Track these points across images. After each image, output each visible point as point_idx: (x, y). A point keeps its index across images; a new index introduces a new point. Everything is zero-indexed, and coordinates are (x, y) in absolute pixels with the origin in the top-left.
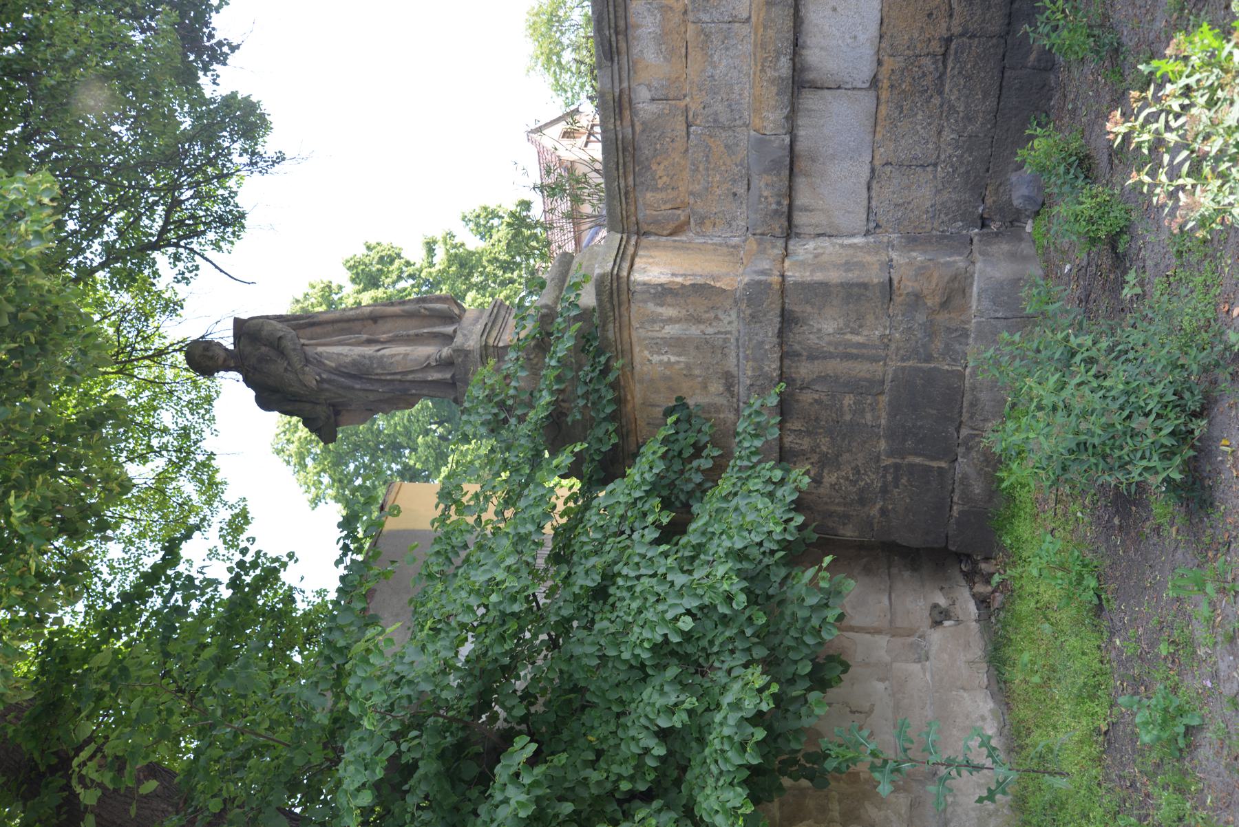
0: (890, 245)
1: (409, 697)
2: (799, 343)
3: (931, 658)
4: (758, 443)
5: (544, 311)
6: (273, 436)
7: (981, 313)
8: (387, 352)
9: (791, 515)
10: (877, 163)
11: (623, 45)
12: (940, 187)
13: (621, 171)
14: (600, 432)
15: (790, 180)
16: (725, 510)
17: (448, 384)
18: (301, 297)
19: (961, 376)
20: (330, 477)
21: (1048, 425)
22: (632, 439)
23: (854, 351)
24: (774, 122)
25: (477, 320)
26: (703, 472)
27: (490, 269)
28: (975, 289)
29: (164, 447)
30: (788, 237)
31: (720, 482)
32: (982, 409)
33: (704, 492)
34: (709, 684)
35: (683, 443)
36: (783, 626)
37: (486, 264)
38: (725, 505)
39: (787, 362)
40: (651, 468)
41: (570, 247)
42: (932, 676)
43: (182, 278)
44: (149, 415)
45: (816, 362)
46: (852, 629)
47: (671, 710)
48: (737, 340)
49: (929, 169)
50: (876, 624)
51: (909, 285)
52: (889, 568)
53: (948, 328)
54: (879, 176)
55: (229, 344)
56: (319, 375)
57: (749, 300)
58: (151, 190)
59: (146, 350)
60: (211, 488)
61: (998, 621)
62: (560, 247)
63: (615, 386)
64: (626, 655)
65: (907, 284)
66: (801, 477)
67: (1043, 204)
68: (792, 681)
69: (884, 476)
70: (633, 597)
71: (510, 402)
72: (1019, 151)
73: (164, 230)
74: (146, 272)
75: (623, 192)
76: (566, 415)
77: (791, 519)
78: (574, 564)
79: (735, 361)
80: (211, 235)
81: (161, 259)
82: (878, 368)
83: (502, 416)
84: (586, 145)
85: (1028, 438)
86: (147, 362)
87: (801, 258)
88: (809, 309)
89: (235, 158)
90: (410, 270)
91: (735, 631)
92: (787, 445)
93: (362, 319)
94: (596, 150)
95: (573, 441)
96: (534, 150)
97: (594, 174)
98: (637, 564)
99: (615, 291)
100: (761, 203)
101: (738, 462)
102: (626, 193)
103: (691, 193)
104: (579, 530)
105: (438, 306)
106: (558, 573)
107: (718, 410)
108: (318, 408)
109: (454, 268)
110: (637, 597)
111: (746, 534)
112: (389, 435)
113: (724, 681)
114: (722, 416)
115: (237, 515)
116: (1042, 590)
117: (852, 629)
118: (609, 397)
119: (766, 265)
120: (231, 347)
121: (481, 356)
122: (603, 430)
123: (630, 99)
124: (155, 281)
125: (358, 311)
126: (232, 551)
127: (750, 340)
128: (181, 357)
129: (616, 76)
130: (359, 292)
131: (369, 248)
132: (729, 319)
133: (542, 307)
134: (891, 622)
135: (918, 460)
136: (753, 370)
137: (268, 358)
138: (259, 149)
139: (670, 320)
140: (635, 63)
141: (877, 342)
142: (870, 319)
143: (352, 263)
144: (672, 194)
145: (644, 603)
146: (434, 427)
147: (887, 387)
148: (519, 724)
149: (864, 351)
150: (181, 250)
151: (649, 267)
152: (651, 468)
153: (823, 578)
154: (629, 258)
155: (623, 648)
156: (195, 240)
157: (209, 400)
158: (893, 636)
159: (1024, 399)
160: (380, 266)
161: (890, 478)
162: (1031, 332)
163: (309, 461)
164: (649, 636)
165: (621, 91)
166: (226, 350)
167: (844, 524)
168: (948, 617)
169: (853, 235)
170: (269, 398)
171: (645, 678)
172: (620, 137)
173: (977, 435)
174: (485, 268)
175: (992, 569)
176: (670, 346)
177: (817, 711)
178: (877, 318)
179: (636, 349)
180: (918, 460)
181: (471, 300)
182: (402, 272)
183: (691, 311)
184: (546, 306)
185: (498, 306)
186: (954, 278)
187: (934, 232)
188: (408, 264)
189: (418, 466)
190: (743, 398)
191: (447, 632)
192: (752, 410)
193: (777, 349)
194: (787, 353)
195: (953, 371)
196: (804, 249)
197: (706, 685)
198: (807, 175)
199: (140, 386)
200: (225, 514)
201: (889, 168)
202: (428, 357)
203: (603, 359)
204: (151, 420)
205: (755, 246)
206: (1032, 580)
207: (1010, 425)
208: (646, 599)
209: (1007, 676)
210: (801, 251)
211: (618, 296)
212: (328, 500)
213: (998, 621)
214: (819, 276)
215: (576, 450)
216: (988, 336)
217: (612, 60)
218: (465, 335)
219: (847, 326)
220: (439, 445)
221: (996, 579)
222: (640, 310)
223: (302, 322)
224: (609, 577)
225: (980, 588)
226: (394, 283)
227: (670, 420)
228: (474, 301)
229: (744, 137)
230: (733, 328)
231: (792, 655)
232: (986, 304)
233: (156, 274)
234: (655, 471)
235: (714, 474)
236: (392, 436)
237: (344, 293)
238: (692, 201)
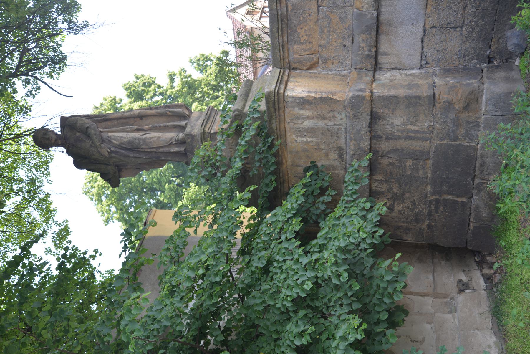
0: (434, 74)
1: (158, 329)
2: (381, 130)
3: (458, 311)
4: (356, 187)
5: (237, 113)
6: (83, 184)
7: (487, 113)
8: (148, 136)
9: (376, 229)
10: (427, 26)
12: (464, 39)
13: (280, 33)
14: (267, 181)
15: (377, 38)
16: (338, 225)
17: (181, 154)
18: (98, 105)
19: (475, 149)
20: (116, 207)
21: (527, 176)
22: (286, 185)
23: (413, 135)
24: (368, 3)
25: (199, 118)
26: (326, 203)
27: (206, 89)
28: (484, 99)
29: (20, 190)
30: (375, 70)
31: (336, 209)
32: (488, 168)
33: (326, 215)
34: (329, 324)
35: (314, 187)
36: (372, 292)
37: (203, 86)
38: (337, 222)
39: (374, 141)
40: (297, 201)
41: (251, 77)
42: (459, 321)
43: (30, 94)
44: (11, 172)
45: (390, 141)
46: (411, 293)
47: (301, 335)
48: (345, 129)
49: (458, 29)
50: (425, 291)
51: (445, 97)
52: (433, 259)
53: (468, 122)
54: (428, 34)
55: (58, 131)
56: (110, 149)
57: (352, 106)
58: (12, 42)
59: (9, 135)
60: (48, 213)
61: (498, 290)
62: (245, 77)
63: (276, 155)
64: (279, 306)
65: (444, 96)
66: (381, 207)
67: (526, 48)
68: (377, 323)
69: (430, 206)
70: (282, 273)
71: (218, 164)
72: (512, 17)
73: (19, 66)
74: (9, 90)
75: (281, 44)
76: (249, 171)
77: (376, 232)
78: (253, 255)
79: (344, 141)
80: (47, 69)
81: (18, 83)
82: (427, 144)
83: (214, 172)
84: (260, 19)
85: (515, 184)
86: (10, 142)
87: (382, 82)
88: (386, 111)
89: (60, 25)
90: (161, 90)
91: (342, 294)
92: (374, 188)
93: (134, 117)
94: (266, 22)
95: (249, 185)
96: (230, 22)
97: (265, 35)
98: (284, 253)
99: (276, 102)
100: (359, 50)
101: (346, 198)
102: (283, 46)
103: (320, 45)
104: (256, 236)
105: (177, 110)
106: (244, 260)
107: (334, 168)
108: (109, 167)
109: (185, 89)
110: (284, 272)
111: (347, 238)
112: (149, 184)
113: (336, 322)
114: (336, 172)
115: (63, 230)
116: (524, 272)
117: (411, 293)
118: (273, 161)
119: (362, 86)
120: (60, 133)
121: (201, 138)
122: (269, 180)
124: (14, 95)
125: (132, 113)
126: (59, 250)
127: (353, 129)
128: (30, 139)
130: (131, 103)
131: (137, 78)
132: (341, 117)
133: (235, 111)
134: (434, 290)
135: (449, 197)
136: (355, 145)
137: (79, 139)
138: (74, 20)
139: (308, 118)
141: (426, 130)
142: (422, 116)
143: (128, 86)
144: (309, 46)
145: (288, 275)
146: (174, 179)
147: (431, 155)
148: (222, 346)
149: (418, 135)
150: (30, 78)
151: (296, 88)
152: (297, 201)
153: (395, 265)
154: (284, 83)
155: (277, 302)
156: (37, 72)
157: (46, 163)
158: (435, 298)
159: (513, 161)
160: (143, 88)
161: (433, 207)
162: (518, 123)
163: (103, 198)
164: (290, 294)
166: (56, 134)
167: (407, 233)
168: (468, 288)
169: (413, 69)
170: (81, 162)
171: (289, 319)
173: (484, 183)
174: (203, 88)
175: (494, 260)
176: (307, 132)
177: (391, 340)
178: (426, 116)
179: (288, 134)
180: (449, 197)
181: (195, 106)
182: (156, 92)
183: (320, 112)
185: (211, 110)
186: (471, 93)
187: (460, 66)
188: (159, 87)
189: (165, 201)
190: (349, 162)
191: (178, 292)
192: (353, 168)
193: (368, 134)
194: (374, 136)
195: (471, 146)
196: (384, 77)
197: (327, 325)
198: (386, 34)
199: (6, 156)
200: (56, 229)
201: (434, 30)
202: (171, 139)
203: (270, 140)
204: (13, 175)
205: (356, 75)
206: (518, 266)
207: (504, 176)
208: (288, 273)
209: (504, 322)
210: (382, 78)
211: (278, 104)
212: (114, 220)
213: (498, 290)
214: (392, 92)
215: (251, 189)
216: (491, 126)
218: (192, 126)
219: (409, 121)
220: (177, 189)
221: (496, 265)
223: (99, 119)
224: (270, 262)
225: (486, 271)
226: (152, 98)
227: (308, 174)
228: (196, 108)
229: (350, 12)
230: (343, 122)
231: (377, 309)
232: (491, 107)
233: (15, 91)
234: (299, 202)
235: (332, 205)
236: (151, 184)
237: (123, 103)
238: (320, 50)
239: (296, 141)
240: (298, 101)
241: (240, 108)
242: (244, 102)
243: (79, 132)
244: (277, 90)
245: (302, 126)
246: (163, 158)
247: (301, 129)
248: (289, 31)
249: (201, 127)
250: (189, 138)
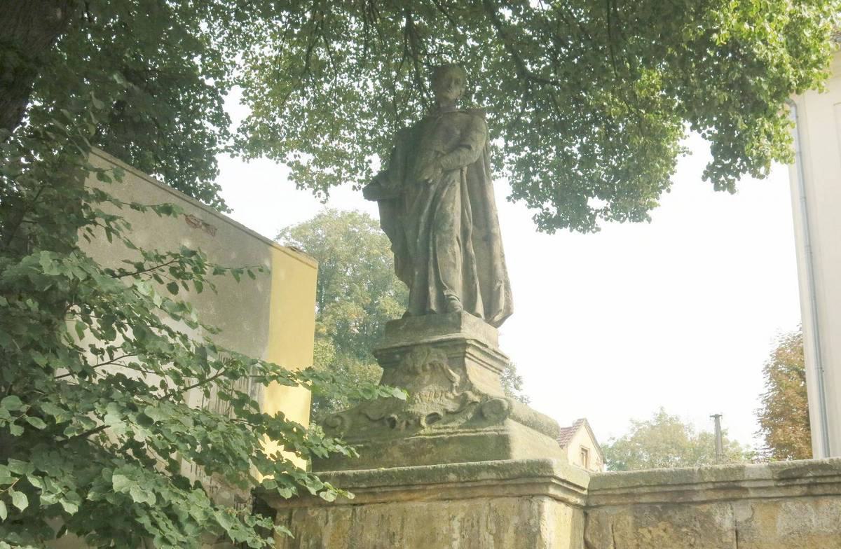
5: (506, 405)
11: (797, 491)
13: (658, 489)
75: (635, 491)
123: (735, 500)
129: (761, 484)
140: (775, 504)
165: (746, 489)
172: (696, 488)
176: (470, 540)
179: (465, 504)
184: (510, 407)
202: (452, 288)
211: (526, 484)
217: (781, 480)
218: (475, 325)
222: (507, 505)
239: (454, 517)
240: (532, 522)
241: (514, 411)
242: (523, 419)
243: (461, 134)
244: (554, 481)
245: (483, 530)
246: (417, 273)
247: (476, 528)
248: (658, 506)
249: (476, 341)
250: (454, 318)
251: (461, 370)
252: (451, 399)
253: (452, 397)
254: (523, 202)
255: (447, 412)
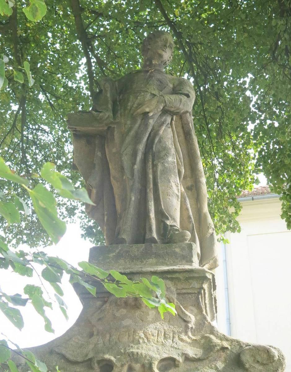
250: (183, 249)
251: (195, 311)
252: (187, 342)
253: (189, 341)
254: (88, 239)
255: (187, 358)
